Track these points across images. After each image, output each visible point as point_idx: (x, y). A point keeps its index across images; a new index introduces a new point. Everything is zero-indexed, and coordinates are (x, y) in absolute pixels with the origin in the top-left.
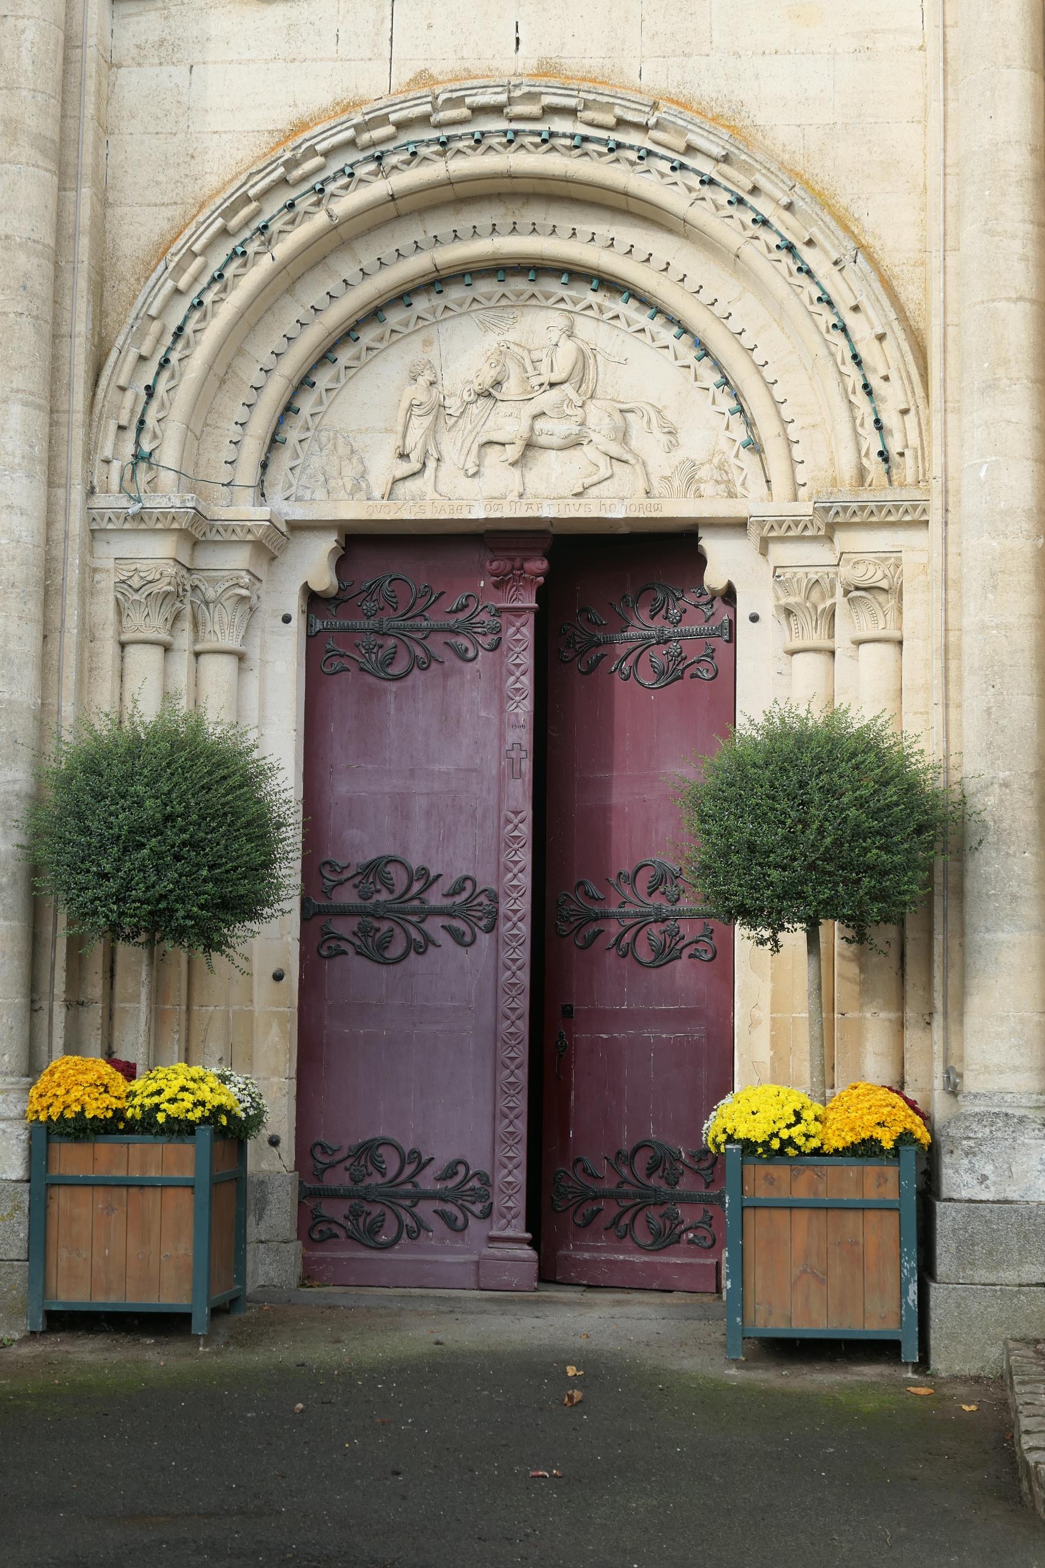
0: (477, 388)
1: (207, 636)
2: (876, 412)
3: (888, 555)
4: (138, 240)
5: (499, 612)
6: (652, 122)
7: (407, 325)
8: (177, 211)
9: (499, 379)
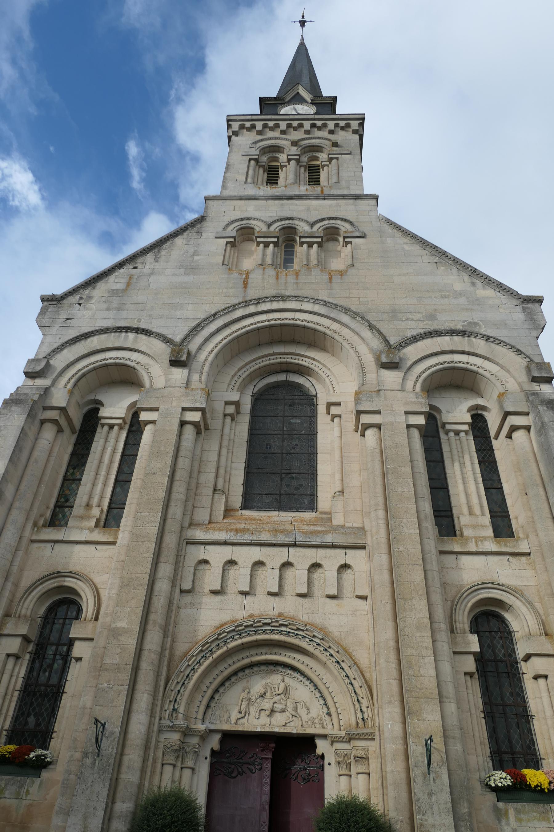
2: (360, 707)
5: (262, 759)
8: (190, 645)
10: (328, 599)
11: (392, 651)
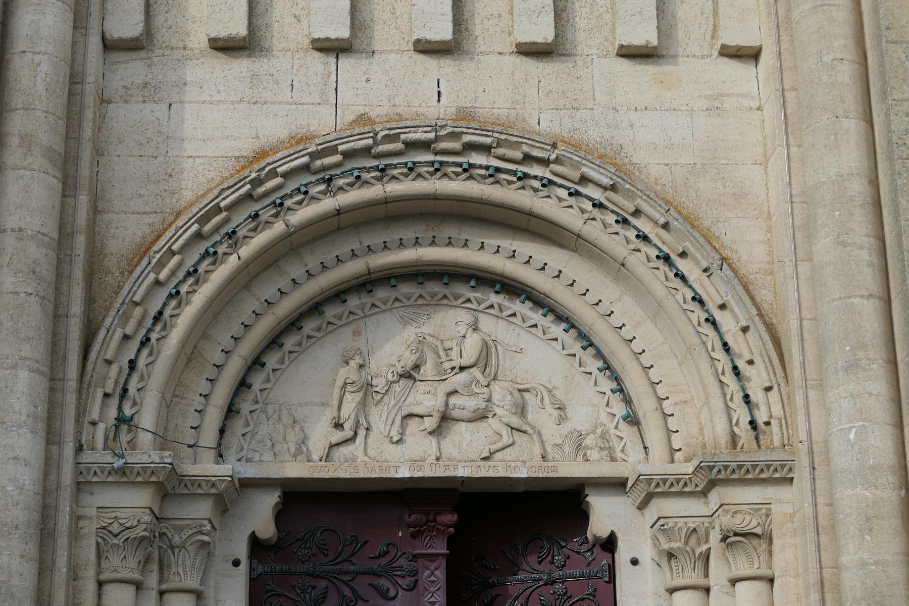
0: (400, 370)
1: (172, 577)
2: (743, 389)
3: (760, 506)
4: (123, 241)
5: (416, 557)
6: (553, 157)
7: (340, 319)
8: (157, 219)
9: (418, 363)
10: (625, 63)
11: (858, 211)
